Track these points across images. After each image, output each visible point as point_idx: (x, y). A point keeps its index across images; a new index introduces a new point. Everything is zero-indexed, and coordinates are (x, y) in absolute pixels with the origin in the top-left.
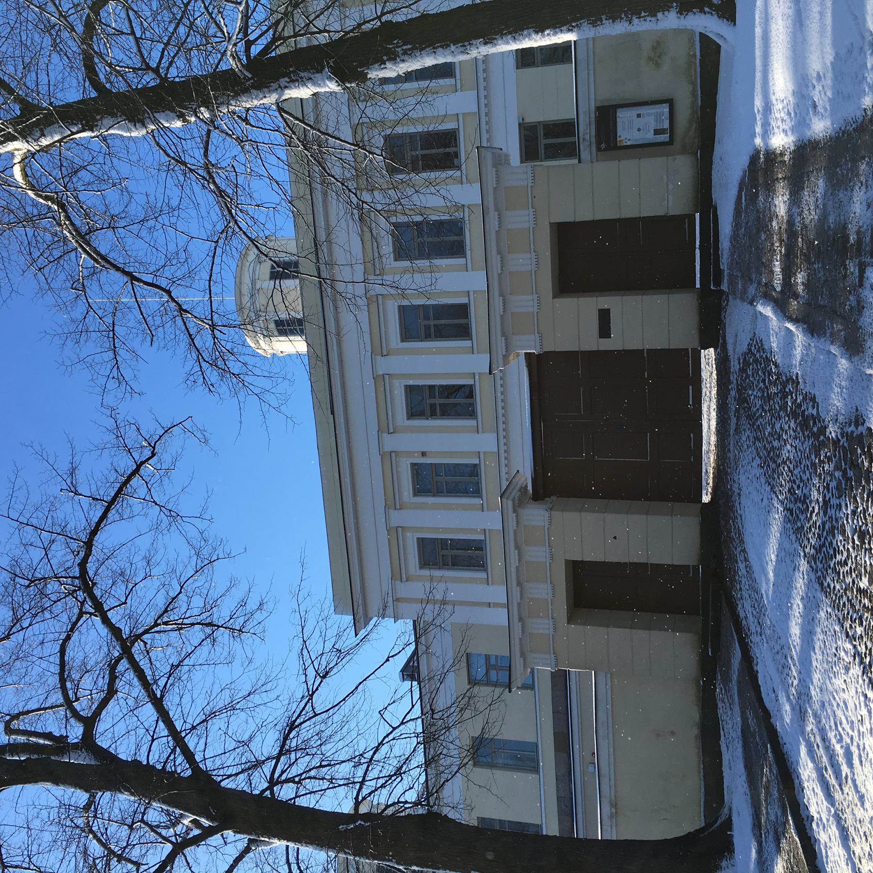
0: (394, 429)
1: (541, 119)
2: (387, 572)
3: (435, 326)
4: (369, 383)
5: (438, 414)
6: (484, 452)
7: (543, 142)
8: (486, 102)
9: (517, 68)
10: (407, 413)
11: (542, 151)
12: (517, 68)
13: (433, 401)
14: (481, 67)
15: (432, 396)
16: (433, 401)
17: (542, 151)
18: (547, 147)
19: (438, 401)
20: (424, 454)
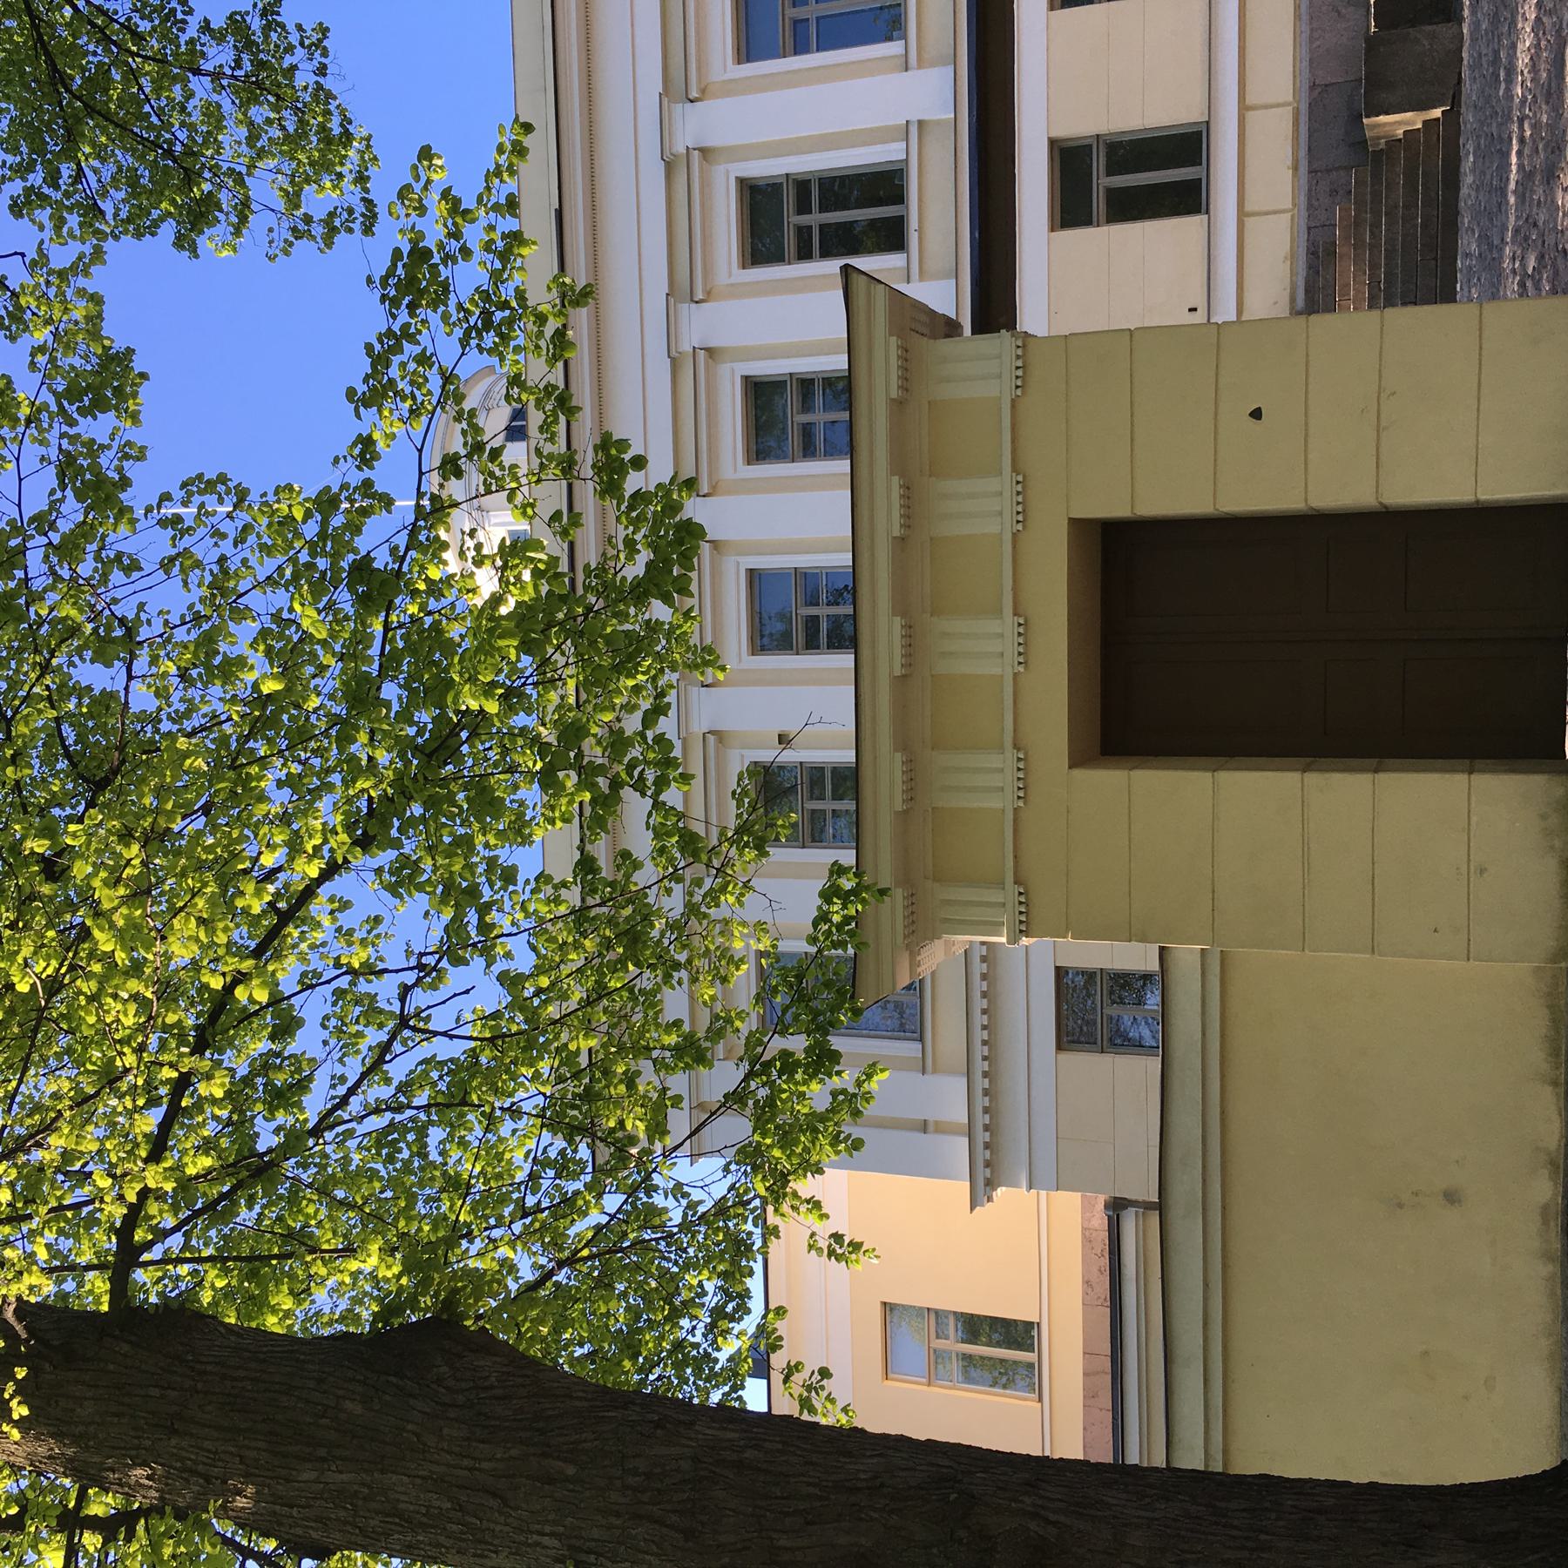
0: (703, 91)
1: (1107, 965)
2: (652, 82)
3: (822, 227)
4: (654, 172)
5: (828, 775)
6: (920, 123)
7: (1102, 182)
8: (988, 1156)
9: (1052, 229)
10: (752, 639)
11: (1099, 204)
12: (1052, 229)
13: (804, 219)
14: (978, 968)
15: (803, 207)
16: (804, 219)
17: (1099, 204)
18: (1111, 193)
19: (815, 219)
20: (784, 740)
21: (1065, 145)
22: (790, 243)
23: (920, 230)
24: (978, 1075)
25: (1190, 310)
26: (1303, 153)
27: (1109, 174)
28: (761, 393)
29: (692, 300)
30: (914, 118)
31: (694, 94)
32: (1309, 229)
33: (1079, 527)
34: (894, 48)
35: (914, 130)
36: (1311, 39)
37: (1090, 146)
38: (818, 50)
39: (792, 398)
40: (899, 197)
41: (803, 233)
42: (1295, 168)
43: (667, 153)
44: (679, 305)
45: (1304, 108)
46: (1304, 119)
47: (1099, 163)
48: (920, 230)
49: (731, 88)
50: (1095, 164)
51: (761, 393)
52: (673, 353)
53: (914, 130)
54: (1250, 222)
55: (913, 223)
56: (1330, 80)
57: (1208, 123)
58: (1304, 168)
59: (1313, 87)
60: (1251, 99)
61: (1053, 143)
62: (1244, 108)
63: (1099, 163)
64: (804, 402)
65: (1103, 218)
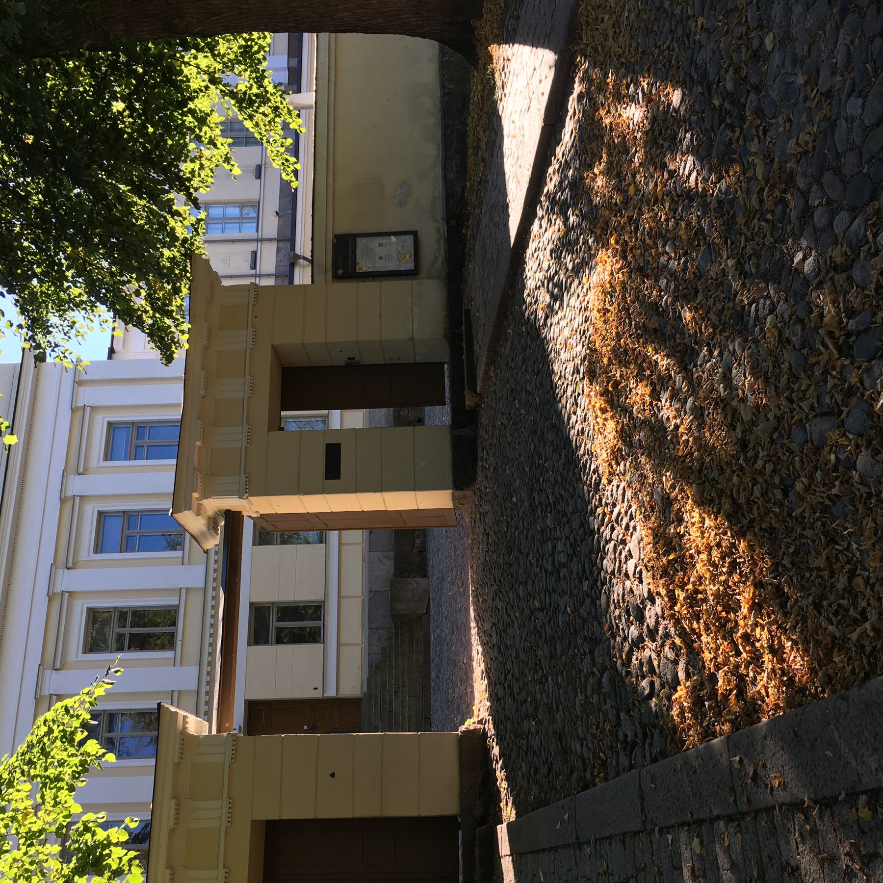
7: (274, 624)
18: (279, 630)
21: (258, 606)
22: (112, 640)
23: (182, 641)
24: (208, 617)
25: (315, 689)
26: (366, 619)
27: (277, 621)
28: (95, 617)
29: (53, 669)
30: (176, 688)
31: (70, 565)
32: (369, 654)
33: (255, 823)
34: (169, 654)
35: (176, 695)
36: (370, 571)
37: (270, 607)
38: (138, 551)
39: (115, 621)
40: (174, 624)
41: (120, 637)
42: (363, 627)
43: (74, 406)
44: (79, 387)
45: (367, 600)
46: (367, 605)
47: (273, 615)
48: (182, 641)
49: (89, 564)
50: (270, 635)
51: (95, 617)
52: (38, 696)
53: (183, 592)
54: (343, 601)
55: (179, 637)
56: (378, 589)
57: (324, 602)
58: (367, 626)
59: (370, 591)
60: (343, 594)
61: (251, 604)
62: (340, 597)
63: (273, 615)
64: (110, 726)
65: (274, 641)
